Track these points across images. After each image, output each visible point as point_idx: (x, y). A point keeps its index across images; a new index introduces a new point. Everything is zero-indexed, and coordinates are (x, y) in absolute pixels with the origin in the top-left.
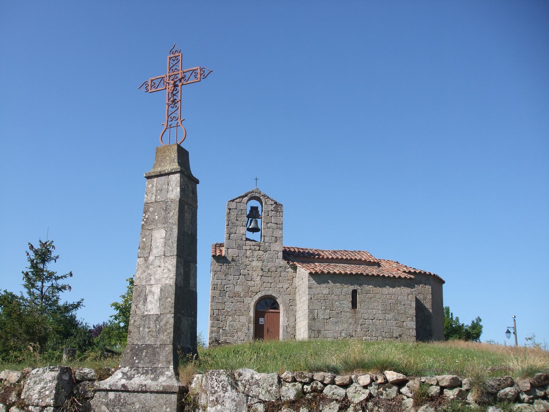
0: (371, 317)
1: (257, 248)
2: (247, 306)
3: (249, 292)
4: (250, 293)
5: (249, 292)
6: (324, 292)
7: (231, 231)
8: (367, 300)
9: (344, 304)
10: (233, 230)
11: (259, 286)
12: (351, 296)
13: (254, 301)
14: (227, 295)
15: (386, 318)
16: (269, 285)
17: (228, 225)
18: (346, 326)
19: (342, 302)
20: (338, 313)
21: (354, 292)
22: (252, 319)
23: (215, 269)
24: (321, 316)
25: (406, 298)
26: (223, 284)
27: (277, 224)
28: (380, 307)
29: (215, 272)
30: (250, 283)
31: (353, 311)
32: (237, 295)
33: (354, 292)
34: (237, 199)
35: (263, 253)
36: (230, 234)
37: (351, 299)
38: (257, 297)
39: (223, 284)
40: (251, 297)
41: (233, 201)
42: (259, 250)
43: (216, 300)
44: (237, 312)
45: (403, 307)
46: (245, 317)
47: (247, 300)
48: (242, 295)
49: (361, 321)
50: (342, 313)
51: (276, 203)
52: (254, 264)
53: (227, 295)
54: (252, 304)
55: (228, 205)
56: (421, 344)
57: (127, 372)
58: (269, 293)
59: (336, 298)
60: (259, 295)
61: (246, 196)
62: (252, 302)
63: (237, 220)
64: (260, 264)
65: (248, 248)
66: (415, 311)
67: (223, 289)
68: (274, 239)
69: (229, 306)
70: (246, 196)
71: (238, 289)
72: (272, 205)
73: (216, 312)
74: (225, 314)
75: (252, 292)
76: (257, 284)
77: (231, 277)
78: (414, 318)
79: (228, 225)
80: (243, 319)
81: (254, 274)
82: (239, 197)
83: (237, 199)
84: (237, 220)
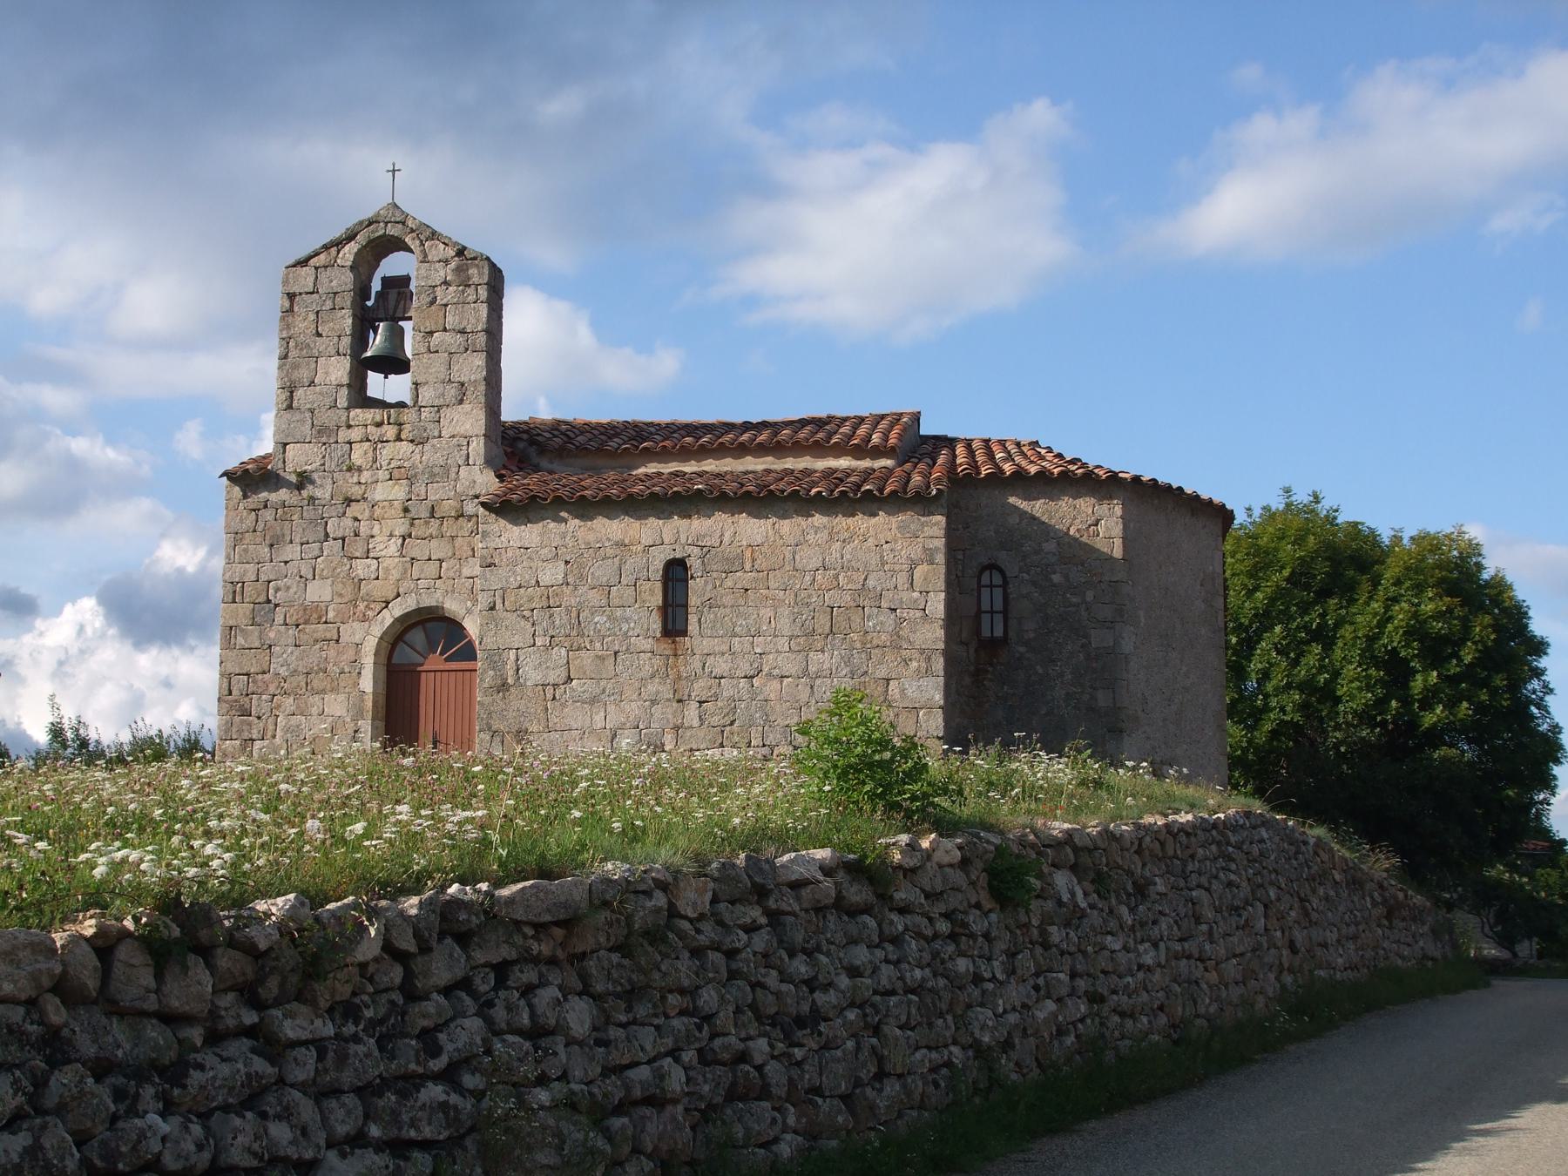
0: (745, 667)
1: (390, 431)
2: (350, 654)
3: (357, 601)
4: (362, 606)
5: (357, 601)
6: (546, 579)
7: (295, 375)
8: (728, 600)
9: (627, 620)
10: (304, 374)
11: (395, 574)
12: (659, 585)
13: (378, 630)
14: (279, 619)
15: (812, 669)
16: (432, 568)
17: (286, 357)
18: (634, 709)
19: (619, 612)
20: (602, 658)
21: (676, 573)
22: (369, 704)
23: (236, 526)
24: (532, 675)
25: (902, 579)
26: (263, 578)
27: (463, 332)
28: (785, 625)
29: (237, 537)
30: (362, 568)
31: (665, 647)
32: (315, 614)
33: (676, 573)
34: (317, 254)
35: (411, 447)
36: (290, 389)
37: (657, 599)
38: (387, 618)
39: (263, 578)
40: (365, 619)
41: (303, 263)
42: (399, 439)
43: (240, 640)
44: (312, 682)
45: (889, 621)
46: (342, 697)
47: (352, 632)
48: (331, 615)
49: (699, 688)
50: (621, 656)
51: (461, 252)
52: (379, 493)
53: (279, 619)
54: (371, 644)
55: (285, 282)
56: (425, 730)
57: (750, 939)
58: (428, 602)
59: (595, 597)
60: (398, 609)
61: (350, 237)
62: (367, 638)
63: (319, 335)
64: (399, 492)
65: (355, 434)
66: (941, 633)
67: (262, 599)
68: (452, 391)
69: (285, 659)
70: (350, 237)
71: (319, 592)
72: (446, 262)
73: (239, 683)
74: (272, 689)
75: (370, 600)
76: (387, 570)
77: (291, 552)
78: (939, 664)
79: (286, 357)
80: (336, 706)
81: (376, 531)
82: (326, 247)
83: (317, 254)
84: (319, 335)
